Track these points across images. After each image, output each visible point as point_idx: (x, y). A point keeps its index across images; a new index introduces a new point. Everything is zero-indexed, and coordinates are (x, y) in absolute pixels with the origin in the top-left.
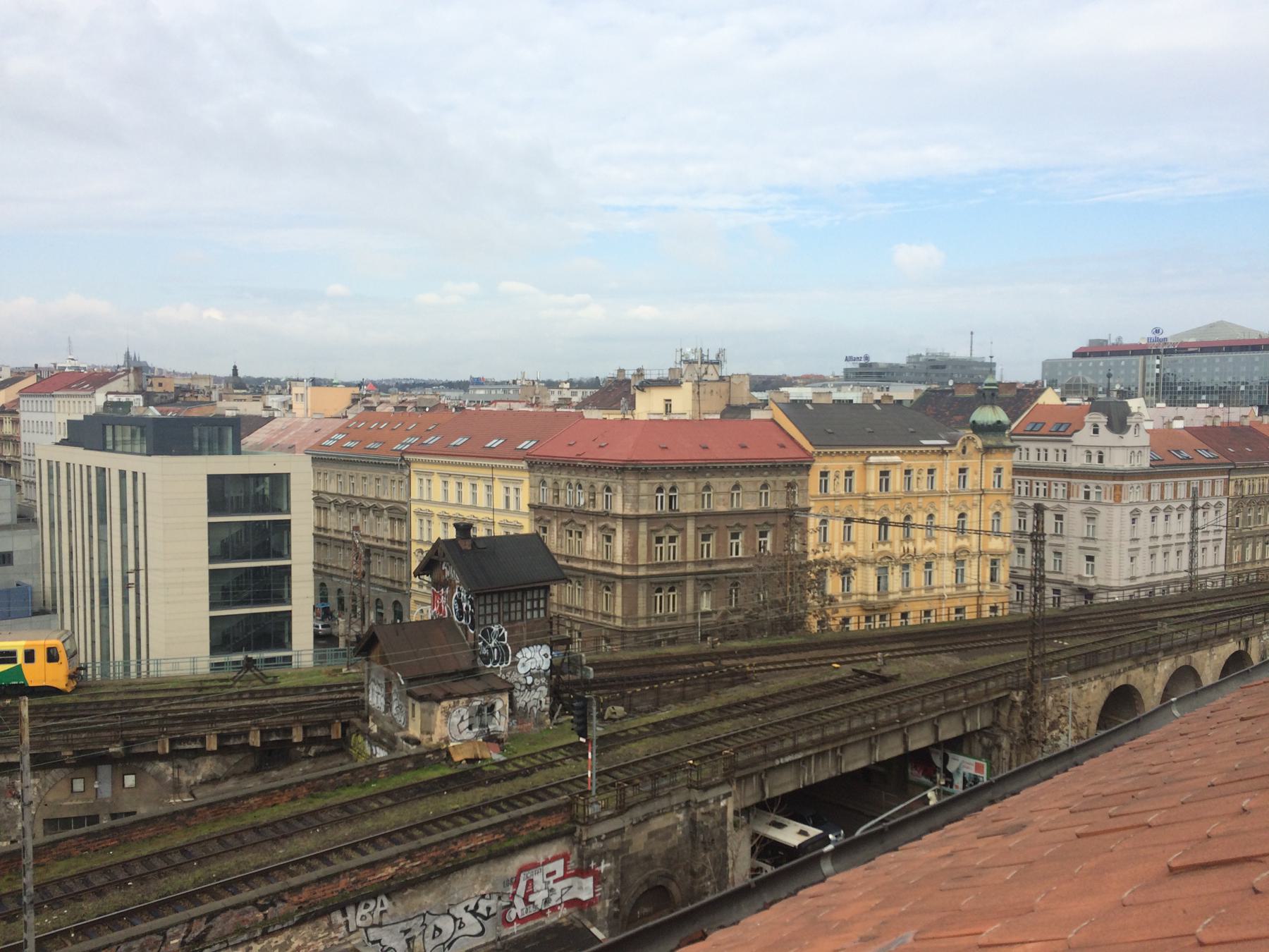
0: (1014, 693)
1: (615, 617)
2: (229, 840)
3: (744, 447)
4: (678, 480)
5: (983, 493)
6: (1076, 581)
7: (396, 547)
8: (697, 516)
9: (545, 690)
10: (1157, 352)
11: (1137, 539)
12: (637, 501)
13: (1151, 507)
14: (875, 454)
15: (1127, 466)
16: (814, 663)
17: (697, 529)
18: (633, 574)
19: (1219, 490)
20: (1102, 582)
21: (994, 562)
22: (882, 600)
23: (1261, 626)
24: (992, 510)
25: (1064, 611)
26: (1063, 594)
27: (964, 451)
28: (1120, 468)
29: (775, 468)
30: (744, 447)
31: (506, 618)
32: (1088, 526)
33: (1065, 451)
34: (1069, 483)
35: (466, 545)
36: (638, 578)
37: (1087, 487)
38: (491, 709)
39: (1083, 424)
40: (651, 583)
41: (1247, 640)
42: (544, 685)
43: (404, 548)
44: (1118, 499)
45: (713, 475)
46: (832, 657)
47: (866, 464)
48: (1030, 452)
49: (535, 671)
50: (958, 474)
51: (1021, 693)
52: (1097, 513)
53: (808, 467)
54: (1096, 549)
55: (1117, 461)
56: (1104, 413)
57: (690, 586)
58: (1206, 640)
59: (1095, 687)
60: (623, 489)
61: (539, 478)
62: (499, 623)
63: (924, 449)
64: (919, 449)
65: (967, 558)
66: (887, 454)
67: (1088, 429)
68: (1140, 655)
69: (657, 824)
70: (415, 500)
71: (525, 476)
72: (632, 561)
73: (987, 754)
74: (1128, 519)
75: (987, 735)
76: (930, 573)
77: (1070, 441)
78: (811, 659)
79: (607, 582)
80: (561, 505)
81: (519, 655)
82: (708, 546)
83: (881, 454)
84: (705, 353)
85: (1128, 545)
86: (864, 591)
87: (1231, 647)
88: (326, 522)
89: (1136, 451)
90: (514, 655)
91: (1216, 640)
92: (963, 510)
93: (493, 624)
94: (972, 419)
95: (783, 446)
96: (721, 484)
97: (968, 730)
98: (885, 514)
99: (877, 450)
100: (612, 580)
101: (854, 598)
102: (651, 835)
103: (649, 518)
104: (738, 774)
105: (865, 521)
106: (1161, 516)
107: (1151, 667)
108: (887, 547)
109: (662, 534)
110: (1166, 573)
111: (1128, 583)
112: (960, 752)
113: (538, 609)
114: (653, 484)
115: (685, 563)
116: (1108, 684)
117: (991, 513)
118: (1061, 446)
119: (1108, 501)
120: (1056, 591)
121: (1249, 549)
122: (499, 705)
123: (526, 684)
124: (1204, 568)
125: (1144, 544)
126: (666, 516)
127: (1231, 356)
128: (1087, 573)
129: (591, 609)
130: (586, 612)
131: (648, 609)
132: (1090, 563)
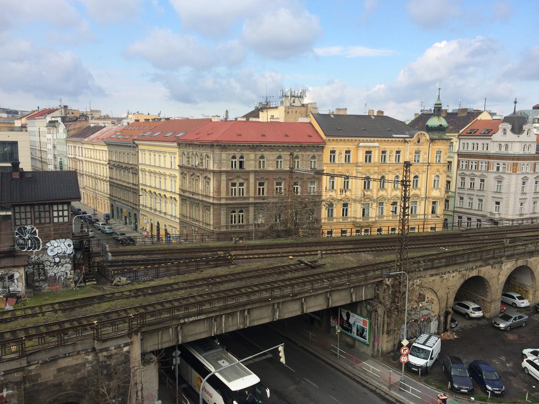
0: (387, 279)
1: (210, 225)
2: (41, 328)
3: (287, 136)
4: (244, 153)
5: (429, 164)
6: (488, 215)
7: (134, 187)
8: (255, 172)
9: (69, 266)
11: (525, 193)
12: (220, 162)
14: (363, 141)
15: (521, 152)
16: (285, 255)
17: (256, 179)
18: (219, 202)
20: (503, 216)
21: (434, 203)
24: (434, 174)
27: (419, 142)
28: (517, 153)
30: (287, 136)
31: (37, 221)
32: (498, 186)
34: (488, 162)
35: (16, 175)
36: (220, 205)
37: (498, 164)
38: (11, 277)
39: (497, 129)
40: (229, 208)
42: (69, 263)
43: (137, 188)
44: (515, 171)
45: (265, 150)
46: (289, 252)
47: (358, 147)
48: (469, 145)
49: (61, 254)
50: (414, 154)
51: (390, 280)
53: (323, 148)
54: (502, 198)
55: (516, 149)
56: (510, 123)
57: (251, 209)
59: (453, 277)
60: (213, 157)
61: (182, 152)
62: (31, 224)
63: (394, 139)
64: (390, 139)
65: (418, 200)
66: (371, 141)
67: (500, 132)
68: (489, 259)
69: (63, 363)
70: (140, 164)
71: (177, 150)
72: (218, 196)
73: (369, 315)
74: (520, 182)
76: (382, 208)
78: (283, 253)
79: (207, 206)
80: (190, 166)
81: (48, 244)
82: (263, 189)
83: (367, 141)
86: (355, 216)
88: (112, 175)
89: (528, 144)
90: (44, 244)
92: (417, 174)
93: (27, 224)
94: (427, 124)
95: (310, 136)
96: (270, 156)
97: (354, 300)
98: (368, 175)
99: (365, 139)
100: (209, 205)
101: (349, 220)
102: (60, 370)
103: (227, 172)
104: (144, 330)
105: (356, 177)
107: (497, 266)
108: (369, 193)
111: (518, 217)
112: (355, 312)
113: (63, 216)
114: (229, 154)
115: (248, 198)
116: (463, 275)
117: (433, 176)
119: (509, 172)
120: (469, 219)
122: (17, 275)
123: (55, 262)
126: (237, 172)
129: (201, 220)
130: (199, 221)
131: (227, 222)
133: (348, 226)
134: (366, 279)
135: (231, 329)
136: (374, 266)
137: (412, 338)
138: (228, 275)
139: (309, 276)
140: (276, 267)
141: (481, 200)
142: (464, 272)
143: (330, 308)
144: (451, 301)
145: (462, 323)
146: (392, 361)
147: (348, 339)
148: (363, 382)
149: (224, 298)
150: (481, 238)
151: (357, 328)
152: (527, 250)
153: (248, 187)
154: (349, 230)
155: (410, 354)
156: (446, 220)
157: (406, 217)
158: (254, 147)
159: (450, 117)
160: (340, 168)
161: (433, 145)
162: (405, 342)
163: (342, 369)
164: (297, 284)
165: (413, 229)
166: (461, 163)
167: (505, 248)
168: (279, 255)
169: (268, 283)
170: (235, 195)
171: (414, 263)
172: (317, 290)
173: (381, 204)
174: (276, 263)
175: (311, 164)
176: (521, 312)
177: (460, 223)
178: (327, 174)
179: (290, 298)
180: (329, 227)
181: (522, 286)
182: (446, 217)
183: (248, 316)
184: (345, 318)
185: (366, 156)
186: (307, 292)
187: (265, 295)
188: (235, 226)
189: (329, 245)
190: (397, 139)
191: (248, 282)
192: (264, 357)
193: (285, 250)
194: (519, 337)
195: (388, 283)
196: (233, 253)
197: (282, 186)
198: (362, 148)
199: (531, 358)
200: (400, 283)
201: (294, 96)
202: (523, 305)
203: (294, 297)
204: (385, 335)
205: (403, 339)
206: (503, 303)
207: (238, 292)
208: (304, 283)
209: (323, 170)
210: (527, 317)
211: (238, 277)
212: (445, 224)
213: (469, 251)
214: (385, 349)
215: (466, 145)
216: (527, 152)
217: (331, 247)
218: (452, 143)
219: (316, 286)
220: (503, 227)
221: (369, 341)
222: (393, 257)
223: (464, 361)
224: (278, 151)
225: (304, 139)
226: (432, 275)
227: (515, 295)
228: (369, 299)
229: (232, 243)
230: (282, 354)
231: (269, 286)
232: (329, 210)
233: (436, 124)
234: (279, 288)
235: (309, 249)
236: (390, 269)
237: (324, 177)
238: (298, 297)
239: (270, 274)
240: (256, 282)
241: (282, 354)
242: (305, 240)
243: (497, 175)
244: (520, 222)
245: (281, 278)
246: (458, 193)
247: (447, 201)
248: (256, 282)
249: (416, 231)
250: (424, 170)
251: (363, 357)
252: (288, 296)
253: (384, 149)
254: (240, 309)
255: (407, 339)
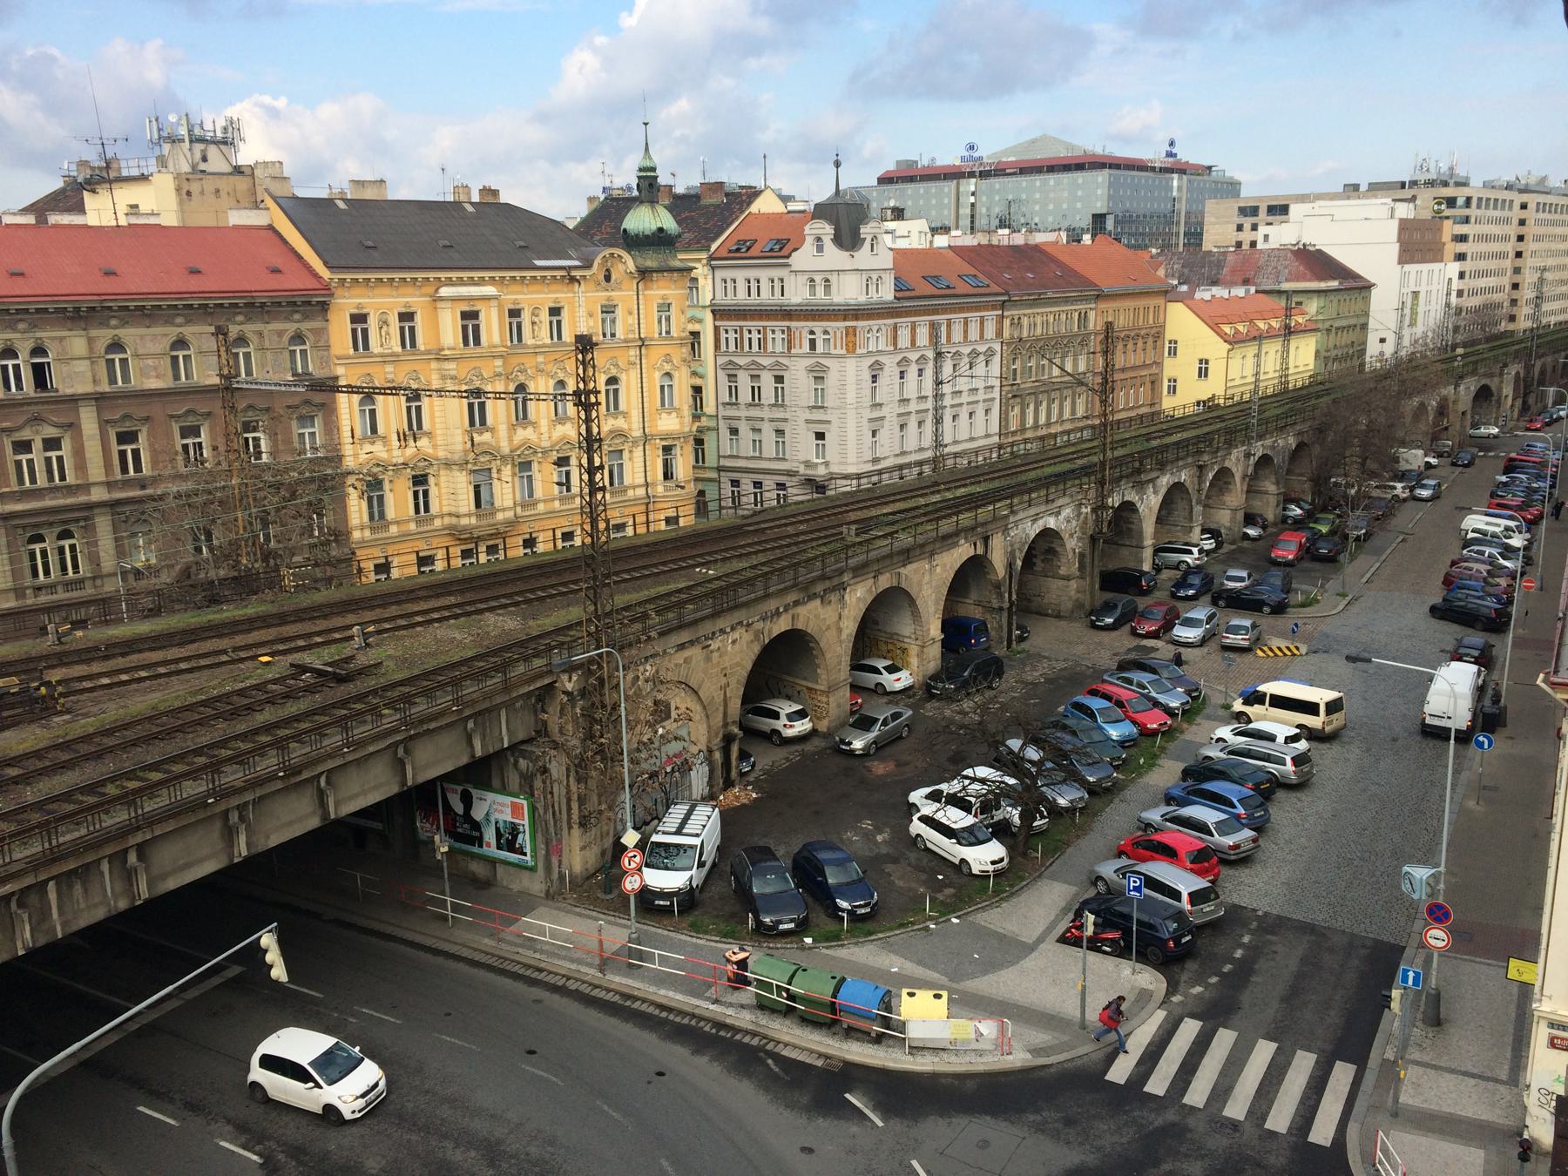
0: (565, 677)
4: (46, 335)
5: (643, 343)
6: (802, 469)
8: (99, 399)
10: (971, 175)
13: (899, 357)
14: (450, 282)
15: (862, 299)
16: (243, 654)
17: (104, 424)
19: (990, 331)
20: (835, 469)
21: (667, 450)
22: (484, 522)
23: (1006, 517)
25: (744, 517)
26: (765, 488)
27: (608, 278)
29: (258, 308)
33: (782, 280)
41: (986, 540)
44: (851, 348)
47: (437, 299)
52: (825, 369)
53: (324, 307)
54: (828, 422)
55: (849, 292)
56: (830, 221)
57: (103, 524)
58: (922, 546)
59: (734, 642)
63: (538, 274)
64: (528, 274)
65: (626, 447)
66: (472, 282)
67: (809, 246)
68: (813, 582)
74: (867, 376)
75: (524, 754)
77: (788, 265)
78: (235, 649)
82: (136, 453)
83: (461, 282)
84: (195, 120)
85: (868, 414)
86: (453, 510)
87: (963, 551)
89: (874, 277)
91: (938, 545)
92: (614, 372)
95: (276, 271)
97: (479, 753)
98: (477, 384)
99: (454, 275)
101: (438, 523)
106: (912, 371)
107: (834, 597)
108: (487, 437)
109: (25, 434)
110: (972, 439)
111: (869, 467)
112: (488, 787)
115: (85, 487)
116: (758, 634)
117: (657, 375)
118: (776, 273)
120: (758, 485)
121: (1030, 410)
124: (956, 442)
125: (890, 411)
126: (28, 402)
127: (1052, 179)
128: (817, 457)
132: (820, 442)
133: (435, 542)
134: (507, 687)
135: (83, 922)
136: (525, 647)
137: (646, 824)
138: (47, 749)
139: (334, 706)
140: (218, 699)
141: (780, 432)
142: (759, 626)
143: (410, 789)
144: (735, 705)
145: (766, 759)
146: (601, 895)
147: (477, 868)
148: (528, 973)
149: (40, 825)
150: (791, 530)
151: (497, 830)
152: (897, 545)
153: (79, 452)
154: (441, 554)
155: (647, 865)
156: (701, 493)
157: (599, 496)
158: (82, 314)
159: (682, 204)
160: (389, 368)
161: (646, 288)
162: (631, 838)
163: (465, 953)
164: (293, 738)
165: (621, 527)
166: (723, 335)
167: (848, 547)
168: (224, 658)
169: (198, 752)
170: (33, 480)
171: (633, 621)
172: (361, 744)
173: (526, 466)
174: (216, 683)
175: (293, 362)
176: (897, 704)
177: (736, 498)
178: (351, 390)
179: (279, 785)
180: (377, 552)
181: (894, 637)
182: (700, 486)
183: (141, 867)
184: (459, 808)
185: (465, 328)
186: (330, 756)
187: (192, 789)
188: (51, 588)
189: (384, 606)
190: (548, 274)
191: (127, 761)
192: (216, 980)
193: (240, 640)
194: (899, 764)
195: (569, 687)
196: (54, 676)
197: (204, 438)
198: (449, 304)
199: (928, 809)
200: (601, 681)
201: (202, 140)
202: (899, 686)
203: (293, 779)
204: (576, 831)
205: (624, 830)
206: (856, 688)
207: (91, 800)
208: (320, 731)
209: (336, 378)
210: (910, 712)
211: (84, 749)
212: (701, 507)
213: (766, 569)
214: (578, 868)
215: (754, 285)
216: (874, 297)
217: (393, 610)
218: (695, 280)
219: (360, 731)
220: (837, 497)
221: (534, 857)
222: (575, 613)
223: (781, 851)
224: (169, 322)
225: (259, 282)
226: (681, 647)
227: (880, 664)
228: (523, 742)
229: (48, 643)
230: (273, 956)
231: (202, 760)
232: (370, 500)
233: (647, 226)
234: (239, 759)
235: (322, 625)
236: (570, 647)
237: (342, 399)
238: (305, 775)
239: (200, 723)
240: (154, 754)
241: (273, 956)
242: (305, 600)
243: (812, 361)
244: (875, 479)
245: (242, 727)
246: (725, 418)
247: (699, 442)
248: (154, 754)
249: (630, 532)
250: (632, 359)
251: (526, 904)
252: (272, 777)
253: (514, 303)
254: (108, 850)
255: (636, 828)
